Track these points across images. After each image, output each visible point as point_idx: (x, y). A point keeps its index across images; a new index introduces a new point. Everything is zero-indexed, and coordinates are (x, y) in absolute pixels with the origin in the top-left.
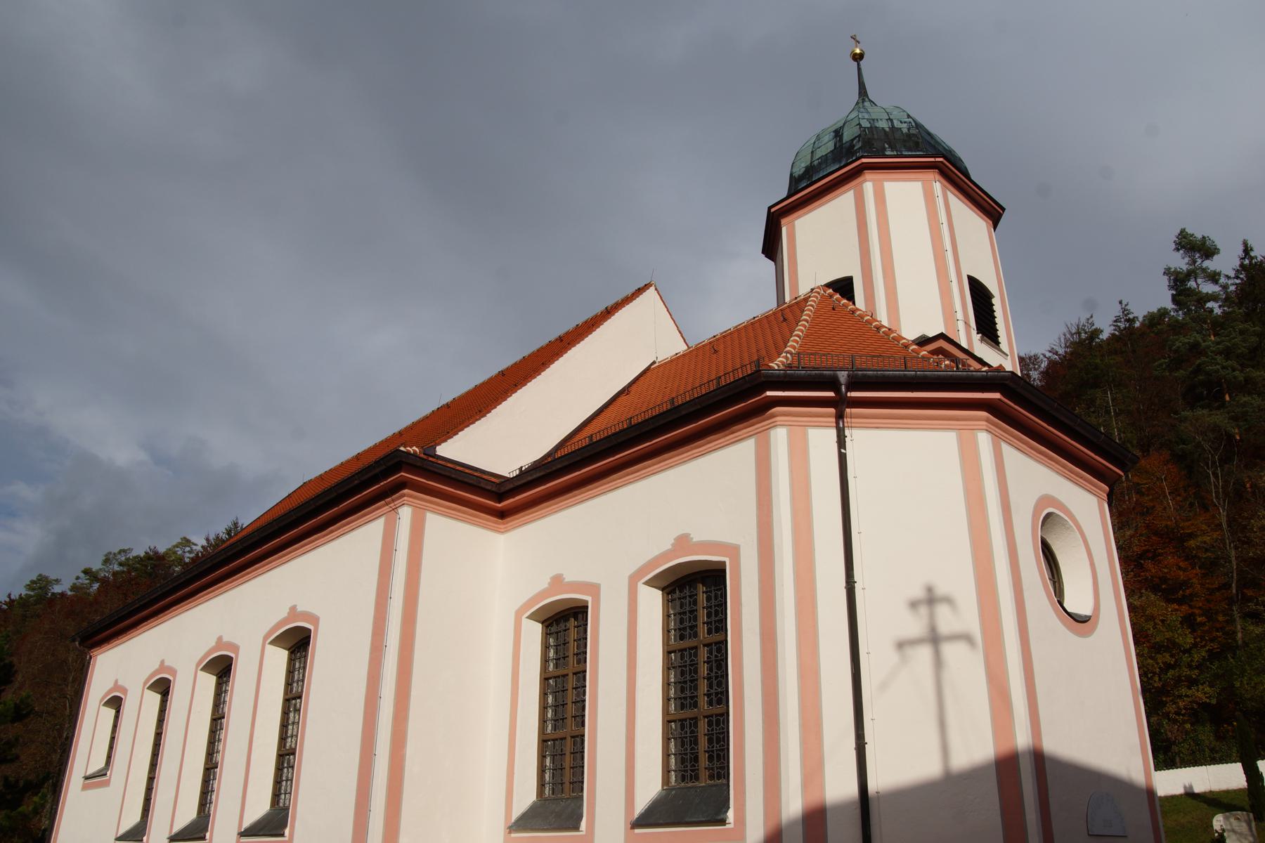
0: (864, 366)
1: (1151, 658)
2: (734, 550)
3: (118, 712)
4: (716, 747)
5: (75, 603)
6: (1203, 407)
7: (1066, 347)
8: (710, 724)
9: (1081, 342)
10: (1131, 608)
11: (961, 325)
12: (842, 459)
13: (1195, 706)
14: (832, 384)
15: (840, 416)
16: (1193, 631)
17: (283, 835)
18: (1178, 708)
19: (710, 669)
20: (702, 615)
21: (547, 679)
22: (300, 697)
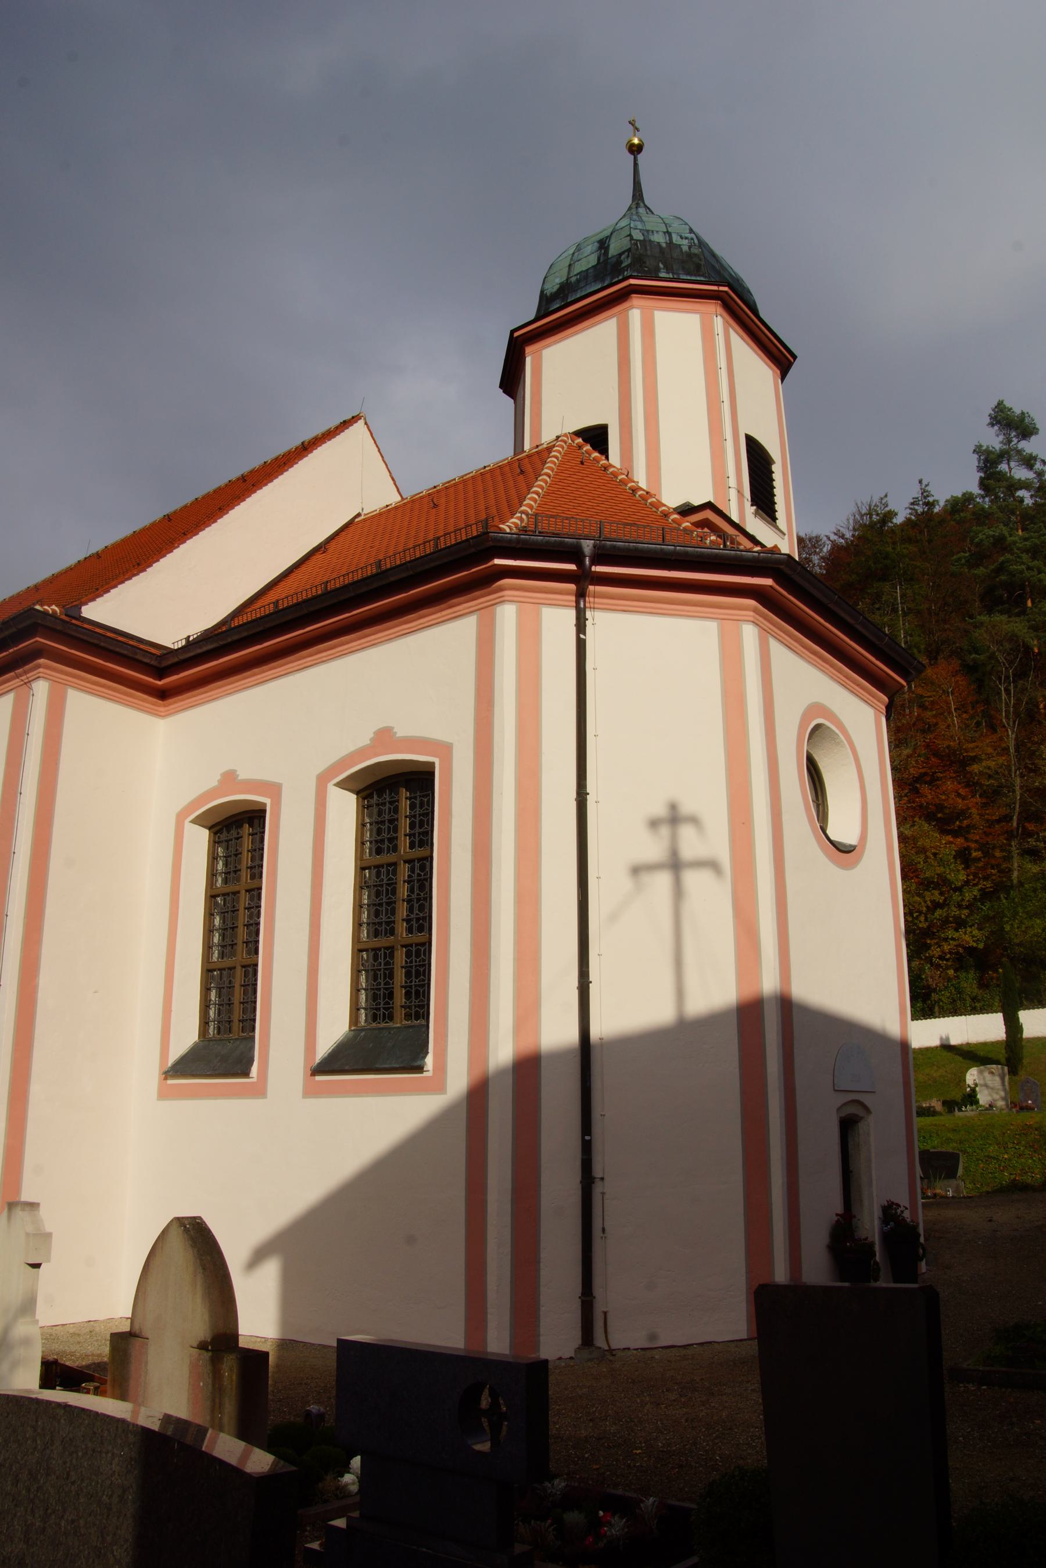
0: (614, 536)
1: (919, 895)
4: (415, 982)
6: (1001, 612)
7: (854, 530)
8: (408, 955)
9: (872, 525)
10: (902, 838)
11: (733, 494)
12: (581, 647)
13: (961, 950)
14: (573, 554)
15: (581, 595)
16: (967, 867)
18: (943, 952)
19: (411, 890)
20: (404, 826)
21: (214, 897)
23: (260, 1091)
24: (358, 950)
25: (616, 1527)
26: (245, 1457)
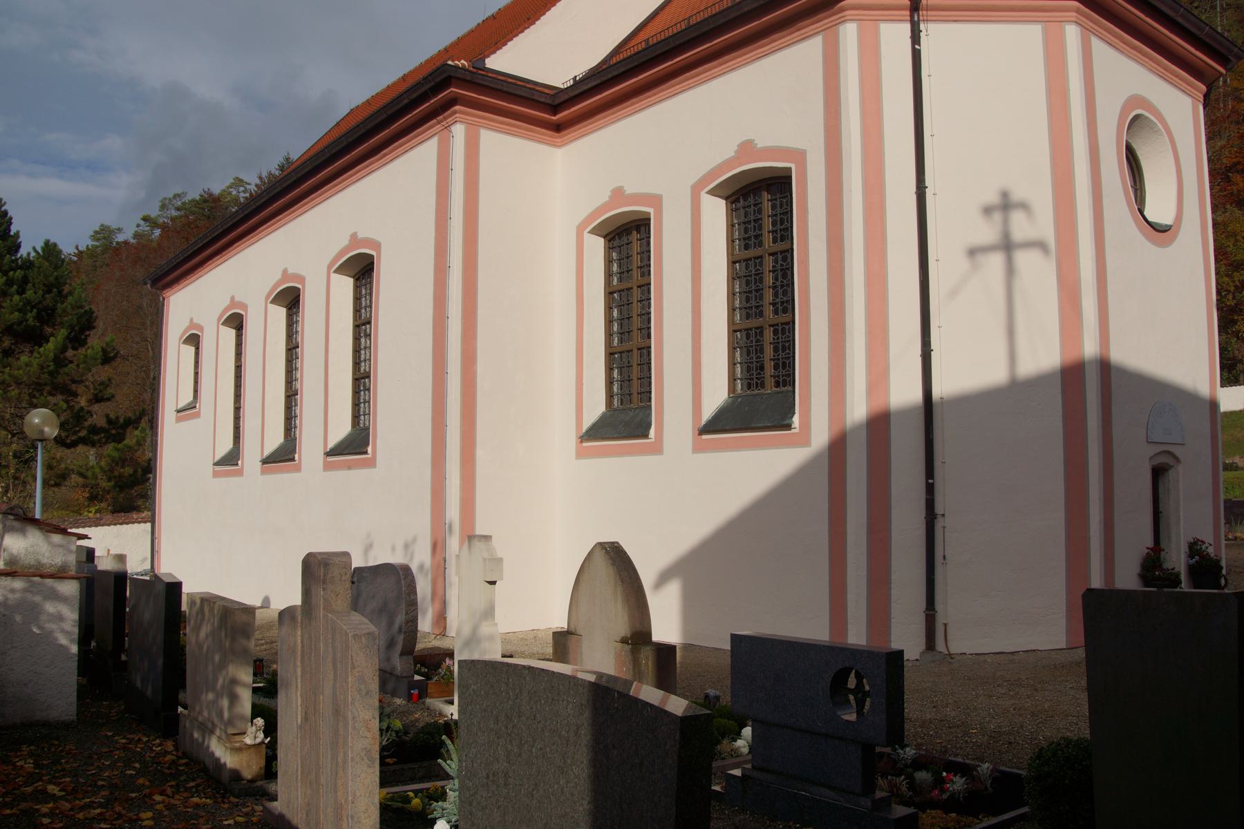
1: (1227, 276)
2: (800, 156)
3: (197, 349)
5: (138, 251)
8: (776, 332)
10: (1215, 225)
17: (366, 453)
20: (767, 224)
21: (611, 293)
22: (369, 323)
23: (657, 449)
24: (733, 331)
25: (958, 784)
26: (664, 701)
